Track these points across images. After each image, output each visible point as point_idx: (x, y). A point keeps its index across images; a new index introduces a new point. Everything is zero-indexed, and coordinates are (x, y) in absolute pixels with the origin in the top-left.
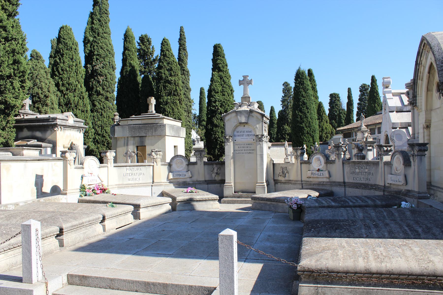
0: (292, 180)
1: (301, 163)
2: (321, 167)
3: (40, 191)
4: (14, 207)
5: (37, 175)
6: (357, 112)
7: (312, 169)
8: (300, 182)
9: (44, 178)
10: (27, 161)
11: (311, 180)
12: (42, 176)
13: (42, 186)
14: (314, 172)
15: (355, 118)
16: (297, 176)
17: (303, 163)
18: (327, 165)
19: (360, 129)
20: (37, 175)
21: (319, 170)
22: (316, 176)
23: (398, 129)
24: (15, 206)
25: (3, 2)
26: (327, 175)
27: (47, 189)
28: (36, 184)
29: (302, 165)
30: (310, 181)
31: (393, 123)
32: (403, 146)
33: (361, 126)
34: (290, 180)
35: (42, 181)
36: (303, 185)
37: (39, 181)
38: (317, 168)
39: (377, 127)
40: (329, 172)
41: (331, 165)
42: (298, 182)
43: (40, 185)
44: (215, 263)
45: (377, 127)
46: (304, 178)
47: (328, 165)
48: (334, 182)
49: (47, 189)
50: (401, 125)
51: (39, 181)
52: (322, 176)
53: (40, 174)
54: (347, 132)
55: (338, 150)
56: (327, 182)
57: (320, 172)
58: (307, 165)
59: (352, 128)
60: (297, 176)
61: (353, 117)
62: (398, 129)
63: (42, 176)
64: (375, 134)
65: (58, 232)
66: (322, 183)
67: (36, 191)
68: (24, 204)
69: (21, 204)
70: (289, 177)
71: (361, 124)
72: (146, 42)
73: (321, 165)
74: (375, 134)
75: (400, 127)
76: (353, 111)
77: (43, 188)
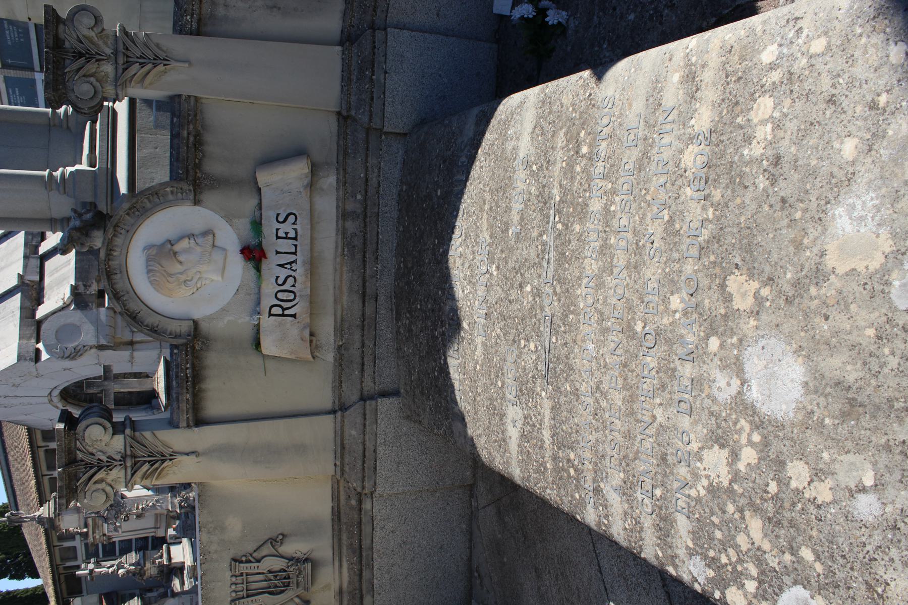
0: (336, 497)
1: (199, 421)
2: (230, 238)
6: (11, 578)
7: (243, 321)
8: (354, 414)
11: (327, 328)
14: (269, 288)
15: (29, 583)
16: (300, 449)
17: (196, 405)
18: (219, 183)
19: (50, 520)
21: (253, 254)
22: (300, 270)
23: (40, 346)
26: (297, 171)
29: (213, 407)
30: (340, 330)
31: (20, 357)
32: (96, 322)
33: (40, 520)
34: (337, 514)
36: (369, 386)
38: (237, 266)
39: (41, 443)
40: (272, 160)
41: (213, 146)
42: (353, 433)
45: (56, 543)
46: (316, 389)
47: (214, 167)
48: (343, 118)
50: (29, 338)
52: (303, 226)
54: (64, 586)
55: (86, 55)
56: (342, 183)
57: (270, 244)
58: (213, 359)
59: (53, 572)
60: (300, 449)
61: (27, 590)
62: (40, 346)
64: (75, 547)
66: (352, 226)
70: (307, 529)
71: (33, 519)
72: (750, 443)
73: (208, 232)
74: (75, 547)
75: (33, 341)
76: (8, 593)
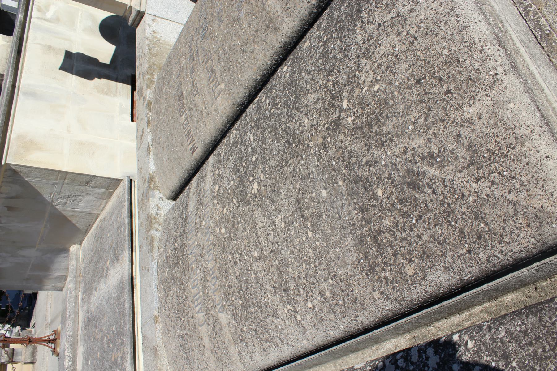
3: (106, 71)
4: (156, 192)
5: (62, 68)
9: (74, 51)
10: (14, 87)
12: (68, 55)
13: (93, 61)
20: (62, 68)
24: (155, 188)
25: (537, 367)
27: (104, 51)
28: (88, 75)
35: (80, 56)
37: (78, 65)
43: (90, 67)
44: (193, 4)
49: (104, 51)
51: (78, 65)
53: (61, 59)
63: (68, 55)
65: (150, 247)
67: (104, 81)
68: (152, 157)
69: (152, 167)
77: (101, 61)
